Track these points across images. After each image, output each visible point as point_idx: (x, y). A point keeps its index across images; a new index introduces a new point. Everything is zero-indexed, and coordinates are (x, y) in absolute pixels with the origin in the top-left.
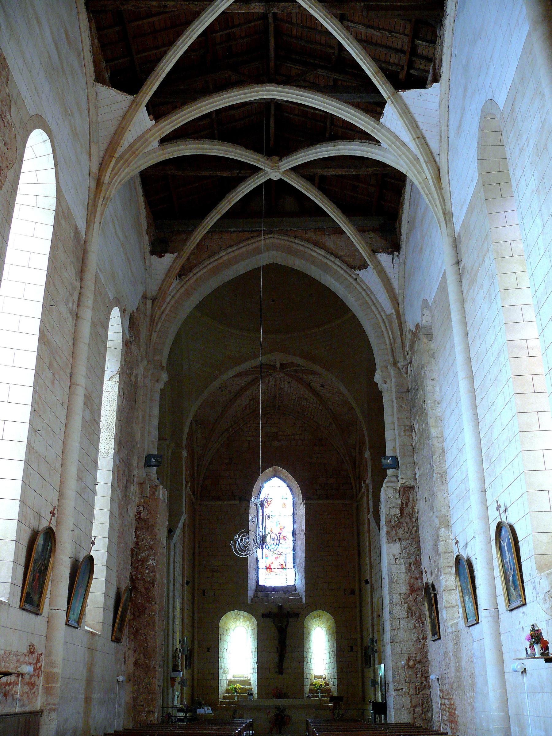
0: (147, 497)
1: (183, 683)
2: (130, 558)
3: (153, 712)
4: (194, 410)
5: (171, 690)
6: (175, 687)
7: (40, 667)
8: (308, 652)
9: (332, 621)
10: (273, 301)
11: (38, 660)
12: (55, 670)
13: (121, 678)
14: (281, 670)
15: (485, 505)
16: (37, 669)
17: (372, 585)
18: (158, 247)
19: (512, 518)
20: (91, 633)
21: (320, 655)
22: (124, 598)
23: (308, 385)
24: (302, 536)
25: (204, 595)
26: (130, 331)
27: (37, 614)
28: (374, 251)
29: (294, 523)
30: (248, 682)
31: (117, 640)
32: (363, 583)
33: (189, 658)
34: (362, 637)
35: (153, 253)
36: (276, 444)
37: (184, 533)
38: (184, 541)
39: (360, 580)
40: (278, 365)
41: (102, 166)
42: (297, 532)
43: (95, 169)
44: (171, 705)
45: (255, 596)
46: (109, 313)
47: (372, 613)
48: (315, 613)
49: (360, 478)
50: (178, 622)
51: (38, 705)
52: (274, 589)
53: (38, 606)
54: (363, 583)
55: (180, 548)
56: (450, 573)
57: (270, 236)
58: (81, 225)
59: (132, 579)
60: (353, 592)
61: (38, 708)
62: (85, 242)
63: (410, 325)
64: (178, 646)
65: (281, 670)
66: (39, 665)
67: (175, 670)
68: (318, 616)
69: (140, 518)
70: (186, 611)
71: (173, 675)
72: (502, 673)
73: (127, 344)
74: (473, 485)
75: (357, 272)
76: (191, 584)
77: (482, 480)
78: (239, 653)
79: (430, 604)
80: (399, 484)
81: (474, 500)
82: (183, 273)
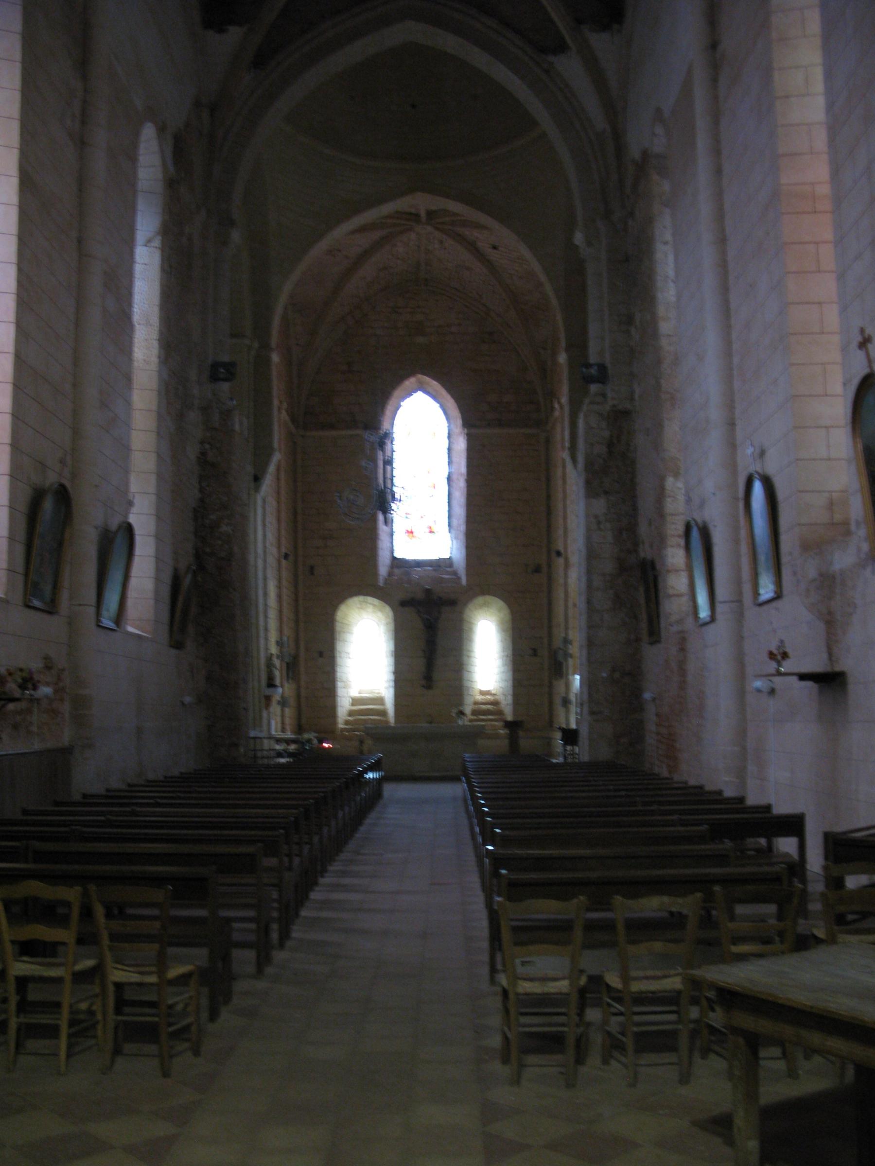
4: (288, 288)
5: (265, 714)
6: (272, 709)
8: (469, 657)
9: (506, 612)
10: (414, 106)
11: (59, 679)
13: (187, 699)
14: (428, 681)
15: (732, 445)
16: (59, 691)
17: (567, 560)
20: (139, 636)
21: (487, 660)
22: (187, 581)
23: (472, 247)
24: (461, 484)
25: (312, 574)
27: (50, 613)
29: (450, 463)
30: (380, 700)
31: (177, 645)
32: (554, 554)
33: (292, 668)
34: (550, 635)
36: (420, 340)
37: (278, 479)
38: (278, 493)
39: (549, 551)
40: (423, 214)
42: (454, 477)
45: (390, 574)
46: (137, 134)
47: (566, 601)
48: (480, 600)
49: (551, 395)
50: (273, 614)
51: (66, 737)
52: (419, 564)
54: (554, 554)
55: (272, 503)
56: (679, 546)
59: (198, 555)
60: (537, 570)
63: (634, 152)
64: (274, 650)
65: (428, 681)
67: (271, 684)
68: (486, 605)
70: (285, 597)
71: (268, 691)
72: (741, 693)
73: (171, 184)
74: (715, 413)
75: (551, 58)
76: (291, 558)
77: (730, 405)
78: (366, 659)
79: (647, 591)
80: (608, 408)
81: (715, 440)
82: (260, 61)
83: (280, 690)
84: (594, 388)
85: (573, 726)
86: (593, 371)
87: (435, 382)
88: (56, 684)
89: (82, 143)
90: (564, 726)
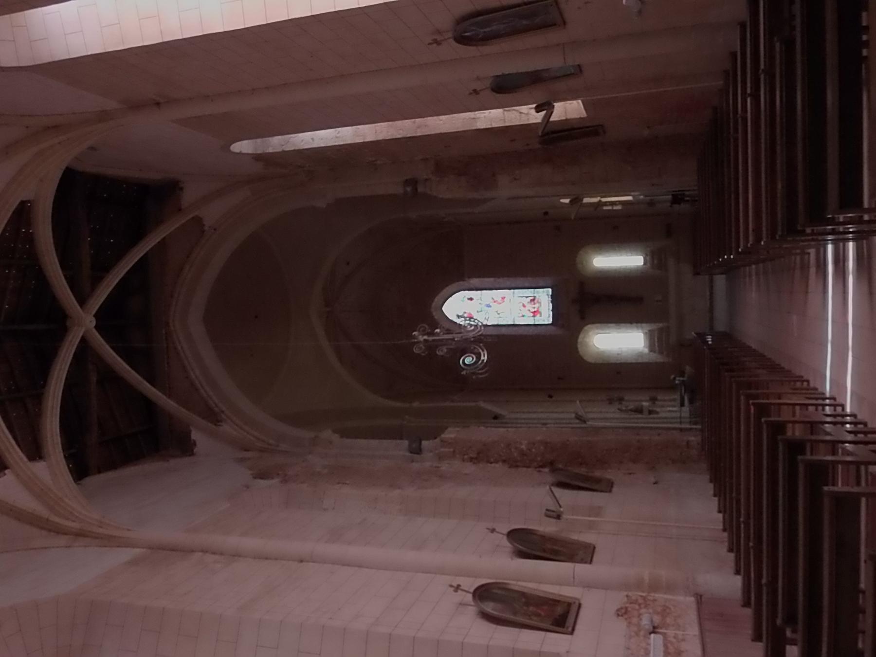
0: (454, 451)
1: (653, 400)
2: (520, 469)
3: (688, 442)
7: (644, 598)
11: (635, 602)
12: (646, 578)
14: (638, 300)
18: (186, 448)
19: (444, 20)
26: (272, 478)
28: (180, 210)
35: (192, 454)
41: (59, 531)
43: (63, 540)
44: (678, 415)
53: (569, 605)
57: (171, 324)
58: (126, 554)
61: (693, 599)
62: (150, 548)
65: (638, 300)
66: (641, 601)
69: (476, 458)
75: (206, 228)
78: (619, 342)
83: (645, 404)
84: (420, 189)
85: (670, 197)
86: (409, 189)
87: (436, 300)
88: (640, 605)
89: (236, 555)
90: (669, 204)
